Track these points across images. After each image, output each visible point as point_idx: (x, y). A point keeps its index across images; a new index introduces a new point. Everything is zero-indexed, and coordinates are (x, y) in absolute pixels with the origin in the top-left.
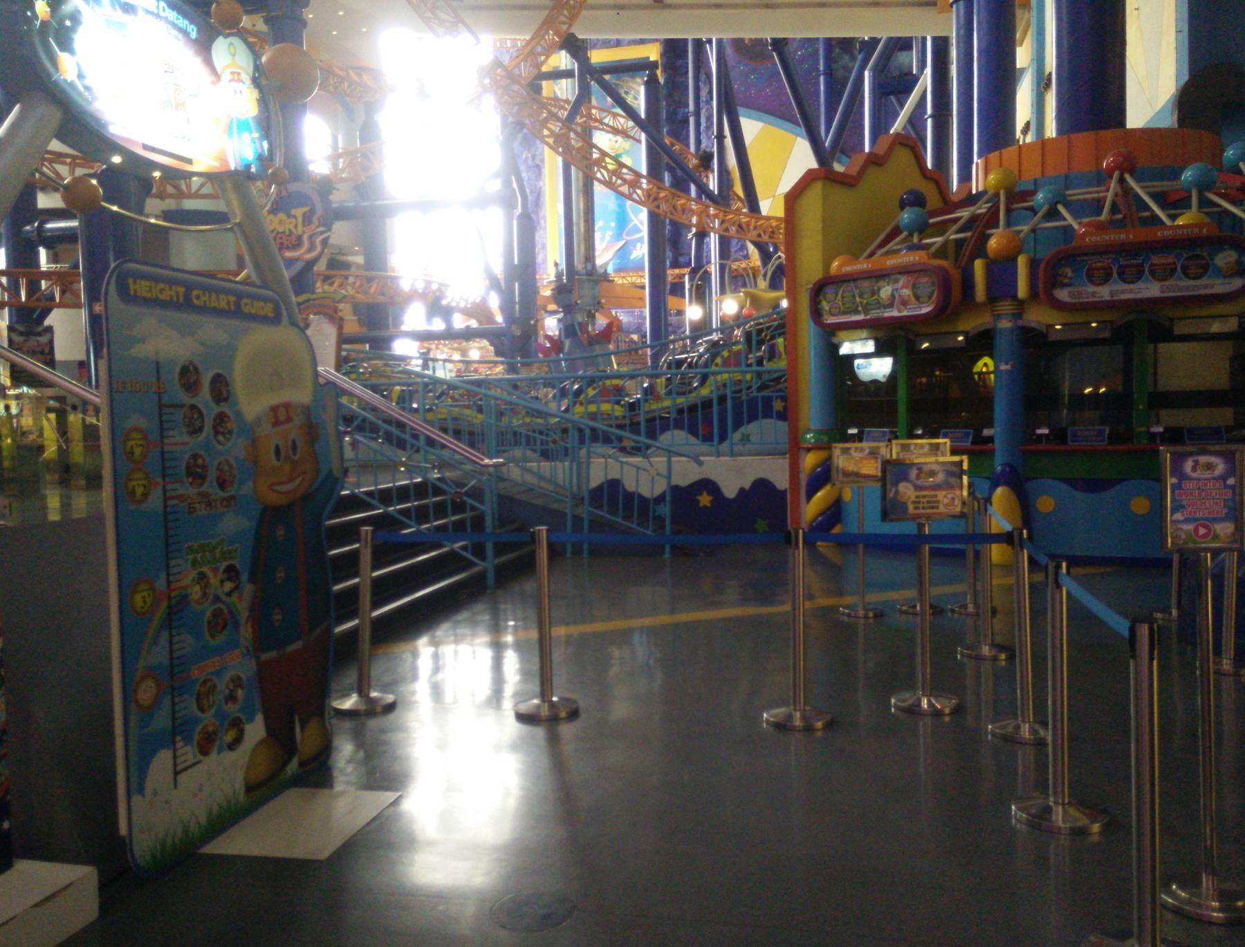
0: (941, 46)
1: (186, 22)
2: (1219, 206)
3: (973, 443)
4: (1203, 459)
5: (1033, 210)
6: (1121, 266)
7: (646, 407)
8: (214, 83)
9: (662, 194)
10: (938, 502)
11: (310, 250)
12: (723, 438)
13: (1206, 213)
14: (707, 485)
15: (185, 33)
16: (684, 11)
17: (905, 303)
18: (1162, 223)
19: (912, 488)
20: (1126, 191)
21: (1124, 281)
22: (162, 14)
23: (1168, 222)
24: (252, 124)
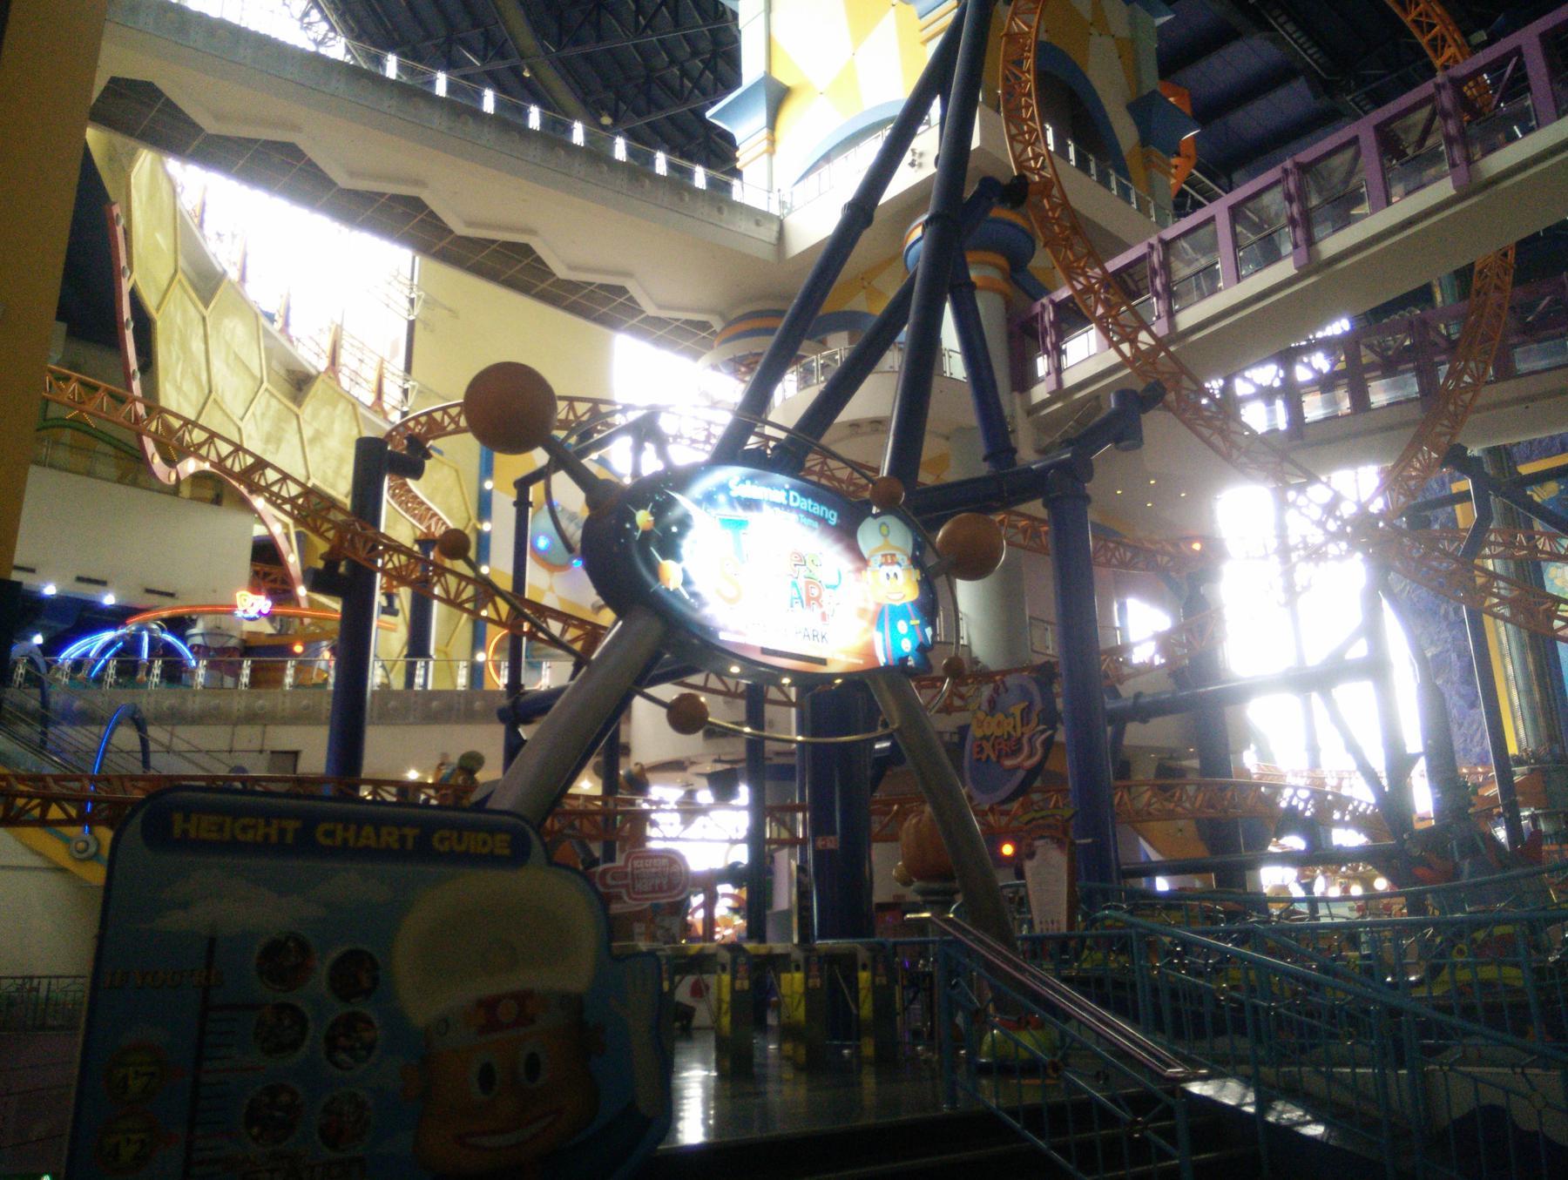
8: (859, 570)
11: (1031, 755)
15: (822, 520)
22: (792, 504)
24: (910, 608)
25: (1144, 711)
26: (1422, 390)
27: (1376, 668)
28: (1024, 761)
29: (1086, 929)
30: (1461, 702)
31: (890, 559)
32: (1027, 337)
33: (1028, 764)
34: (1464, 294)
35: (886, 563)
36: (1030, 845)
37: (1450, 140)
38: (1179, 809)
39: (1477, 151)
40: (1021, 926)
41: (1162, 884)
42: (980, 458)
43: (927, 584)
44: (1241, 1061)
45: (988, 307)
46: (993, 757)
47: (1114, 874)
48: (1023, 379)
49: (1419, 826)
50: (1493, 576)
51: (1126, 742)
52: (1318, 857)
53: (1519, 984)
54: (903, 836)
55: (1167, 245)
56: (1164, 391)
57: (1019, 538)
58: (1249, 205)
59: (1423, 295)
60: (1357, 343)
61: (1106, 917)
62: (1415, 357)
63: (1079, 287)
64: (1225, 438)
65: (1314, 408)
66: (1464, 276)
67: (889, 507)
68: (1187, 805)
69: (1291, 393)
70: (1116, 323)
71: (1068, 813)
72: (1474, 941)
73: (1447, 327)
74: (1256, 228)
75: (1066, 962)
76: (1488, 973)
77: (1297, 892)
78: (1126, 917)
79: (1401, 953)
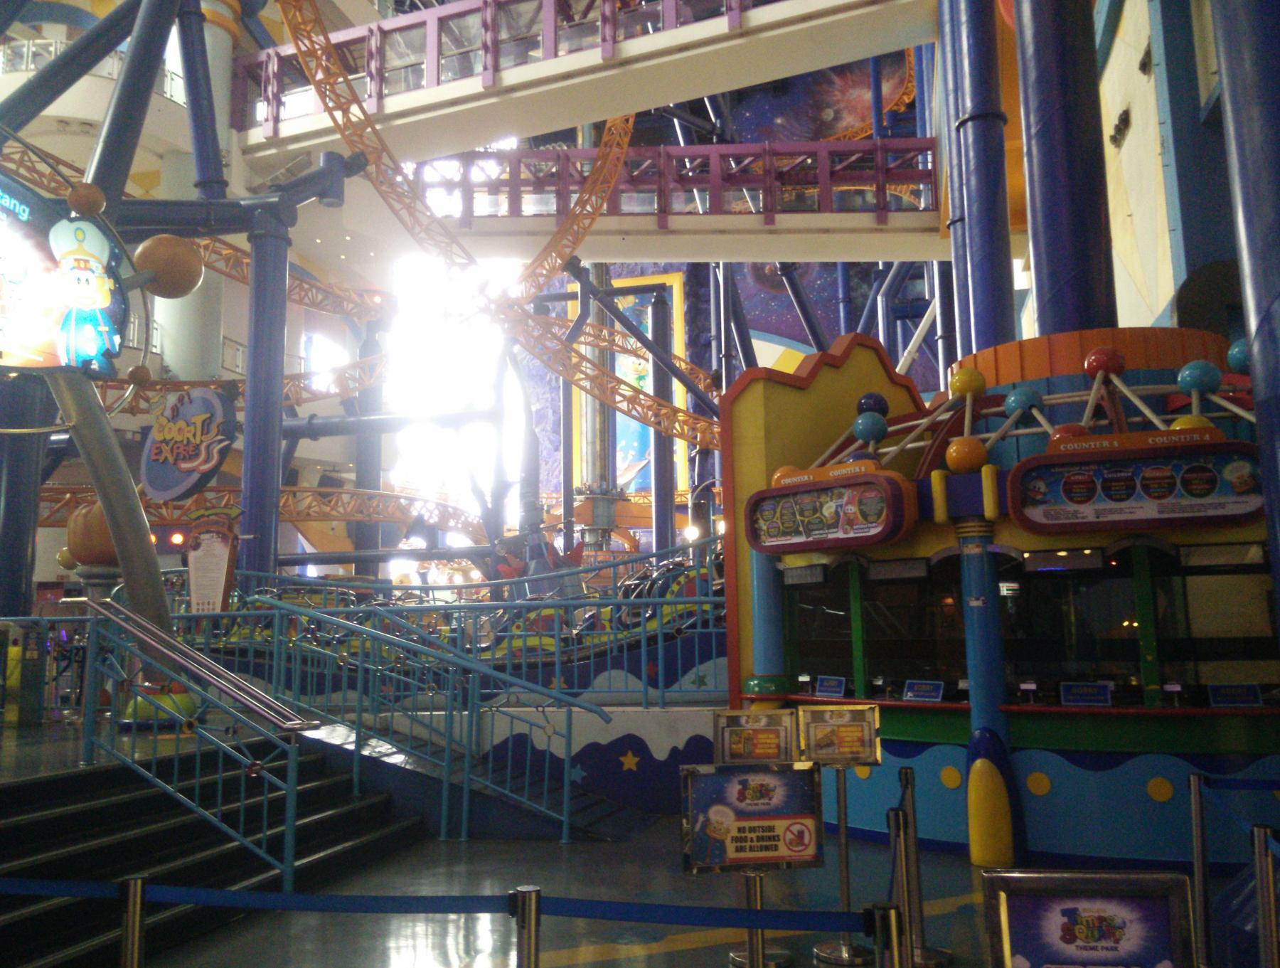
0: (945, 268)
1: (14, 201)
2: (1225, 410)
3: (945, 698)
4: (1090, 909)
5: (1004, 415)
6: (1105, 481)
7: (588, 642)
9: (664, 411)
10: (776, 838)
11: (207, 461)
12: (671, 679)
13: (1212, 419)
14: (633, 743)
15: (11, 213)
16: (686, 237)
17: (851, 523)
18: (1156, 428)
19: (731, 814)
20: (1112, 392)
21: (1110, 497)
23: (1161, 426)
24: (99, 316)
25: (314, 431)
26: (558, 210)
27: (495, 416)
28: (201, 465)
29: (238, 609)
30: (550, 446)
31: (82, 265)
32: (248, 80)
33: (205, 467)
34: (596, 144)
35: (79, 268)
36: (197, 538)
37: (605, 19)
38: (334, 513)
39: (621, 34)
40: (180, 606)
41: (312, 571)
42: (191, 185)
43: (120, 293)
44: (351, 710)
45: (216, 43)
46: (171, 459)
47: (272, 564)
48: (242, 120)
49: (508, 535)
50: (583, 358)
51: (297, 454)
52: (435, 554)
53: (552, 649)
54: (71, 524)
55: (385, 34)
56: (367, 163)
57: (221, 265)
58: (456, 21)
59: (568, 135)
60: (520, 162)
61: (257, 600)
62: (556, 182)
63: (304, 48)
64: (411, 214)
65: (483, 204)
66: (599, 127)
67: (88, 213)
68: (341, 510)
69: (468, 189)
70: (333, 91)
71: (234, 512)
72: (528, 619)
73: (582, 166)
74: (458, 42)
75: (216, 636)
76: (533, 641)
77: (416, 581)
78: (276, 602)
79: (478, 627)
